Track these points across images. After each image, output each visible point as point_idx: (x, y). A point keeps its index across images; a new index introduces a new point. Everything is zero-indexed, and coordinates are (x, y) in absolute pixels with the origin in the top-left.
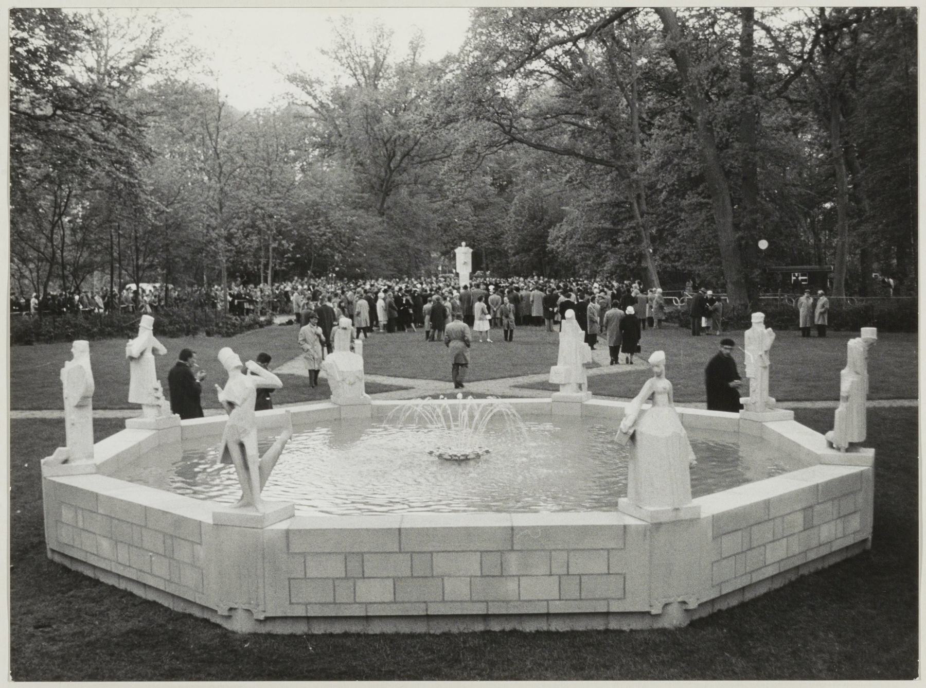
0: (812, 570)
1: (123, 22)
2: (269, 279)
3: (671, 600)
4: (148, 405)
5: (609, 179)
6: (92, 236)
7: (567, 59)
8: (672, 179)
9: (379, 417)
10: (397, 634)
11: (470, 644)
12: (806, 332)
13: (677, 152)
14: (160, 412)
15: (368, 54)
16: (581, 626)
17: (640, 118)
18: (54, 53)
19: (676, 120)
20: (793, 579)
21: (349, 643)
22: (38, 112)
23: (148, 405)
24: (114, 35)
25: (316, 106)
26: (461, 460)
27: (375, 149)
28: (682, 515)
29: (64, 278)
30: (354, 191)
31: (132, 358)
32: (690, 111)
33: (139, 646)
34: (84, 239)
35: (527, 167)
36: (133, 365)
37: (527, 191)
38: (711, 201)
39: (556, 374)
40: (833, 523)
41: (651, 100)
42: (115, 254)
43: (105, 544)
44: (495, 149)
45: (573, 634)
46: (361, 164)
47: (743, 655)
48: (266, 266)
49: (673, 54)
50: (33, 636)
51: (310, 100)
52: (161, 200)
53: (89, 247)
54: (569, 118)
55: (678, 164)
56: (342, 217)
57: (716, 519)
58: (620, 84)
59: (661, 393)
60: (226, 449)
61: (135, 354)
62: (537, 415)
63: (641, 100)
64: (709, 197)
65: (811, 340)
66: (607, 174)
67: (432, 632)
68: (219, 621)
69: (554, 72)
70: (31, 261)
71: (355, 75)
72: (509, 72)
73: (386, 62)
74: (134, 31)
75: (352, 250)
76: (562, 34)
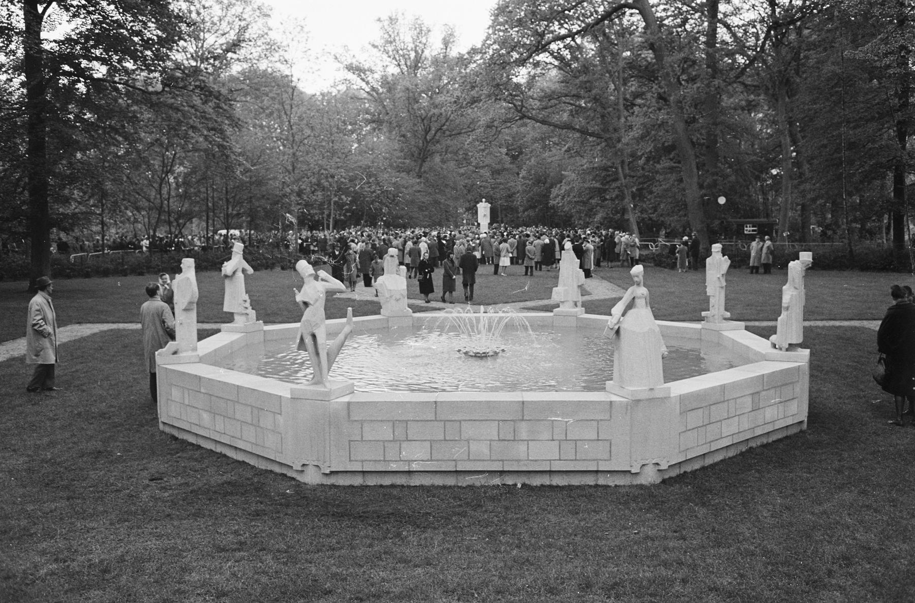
0: (759, 444)
1: (216, 19)
2: (331, 226)
3: (647, 462)
4: (238, 314)
5: (599, 148)
6: (192, 190)
7: (567, 52)
8: (650, 147)
9: (416, 329)
10: (433, 486)
11: (489, 493)
12: (755, 270)
13: (654, 126)
14: (247, 319)
15: (409, 48)
16: (575, 481)
17: (625, 99)
18: (161, 41)
19: (654, 100)
20: (744, 450)
21: (395, 493)
22: (150, 89)
23: (238, 314)
24: (209, 31)
25: (368, 90)
26: (481, 357)
27: (415, 125)
28: (658, 394)
29: (170, 223)
30: (398, 158)
31: (226, 276)
32: (665, 92)
33: (232, 494)
34: (185, 192)
35: (535, 140)
36: (227, 282)
37: (533, 160)
38: (680, 165)
39: (558, 293)
40: (775, 407)
41: (633, 86)
42: (210, 204)
43: (206, 416)
44: (509, 124)
45: (570, 488)
46: (404, 136)
47: (703, 504)
48: (329, 216)
49: (652, 47)
50: (148, 486)
51: (364, 85)
52: (246, 160)
53: (190, 198)
54: (568, 99)
55: (655, 135)
56: (389, 179)
57: (682, 398)
58: (609, 72)
59: (639, 298)
60: (302, 339)
61: (229, 273)
62: (540, 327)
63: (625, 84)
64: (679, 162)
65: (759, 277)
66: (598, 144)
67: (460, 484)
68: (294, 475)
69: (556, 63)
70: (143, 209)
71: (399, 65)
72: (522, 62)
73: (424, 55)
74: (224, 26)
75: (397, 204)
76: (563, 32)
